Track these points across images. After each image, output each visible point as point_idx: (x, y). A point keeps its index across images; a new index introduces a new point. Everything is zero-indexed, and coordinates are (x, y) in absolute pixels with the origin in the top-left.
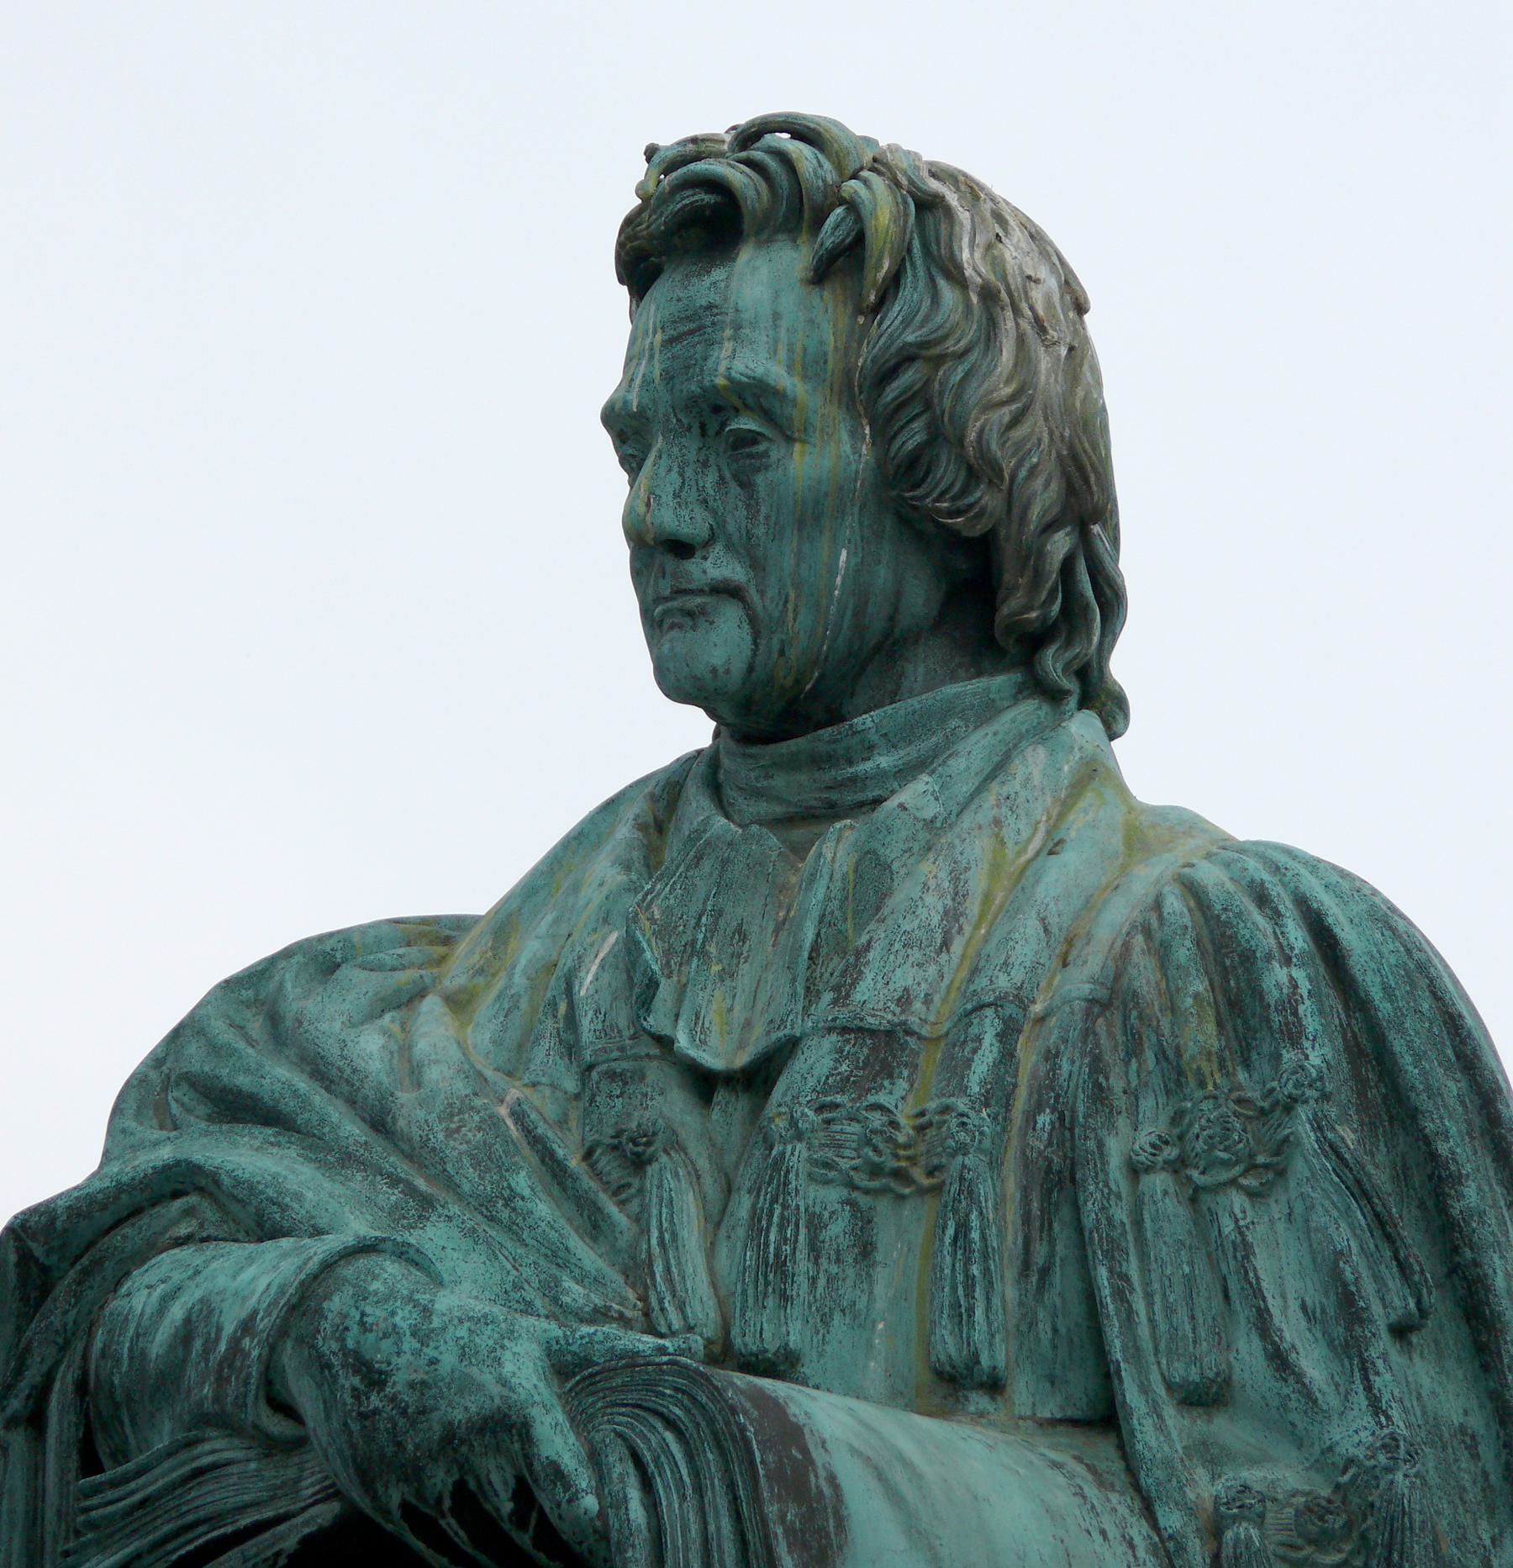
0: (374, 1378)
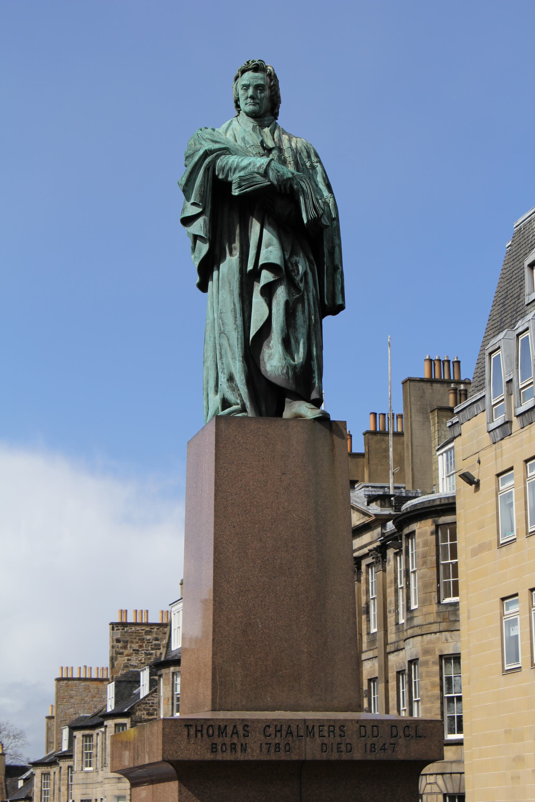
0: (279, 172)
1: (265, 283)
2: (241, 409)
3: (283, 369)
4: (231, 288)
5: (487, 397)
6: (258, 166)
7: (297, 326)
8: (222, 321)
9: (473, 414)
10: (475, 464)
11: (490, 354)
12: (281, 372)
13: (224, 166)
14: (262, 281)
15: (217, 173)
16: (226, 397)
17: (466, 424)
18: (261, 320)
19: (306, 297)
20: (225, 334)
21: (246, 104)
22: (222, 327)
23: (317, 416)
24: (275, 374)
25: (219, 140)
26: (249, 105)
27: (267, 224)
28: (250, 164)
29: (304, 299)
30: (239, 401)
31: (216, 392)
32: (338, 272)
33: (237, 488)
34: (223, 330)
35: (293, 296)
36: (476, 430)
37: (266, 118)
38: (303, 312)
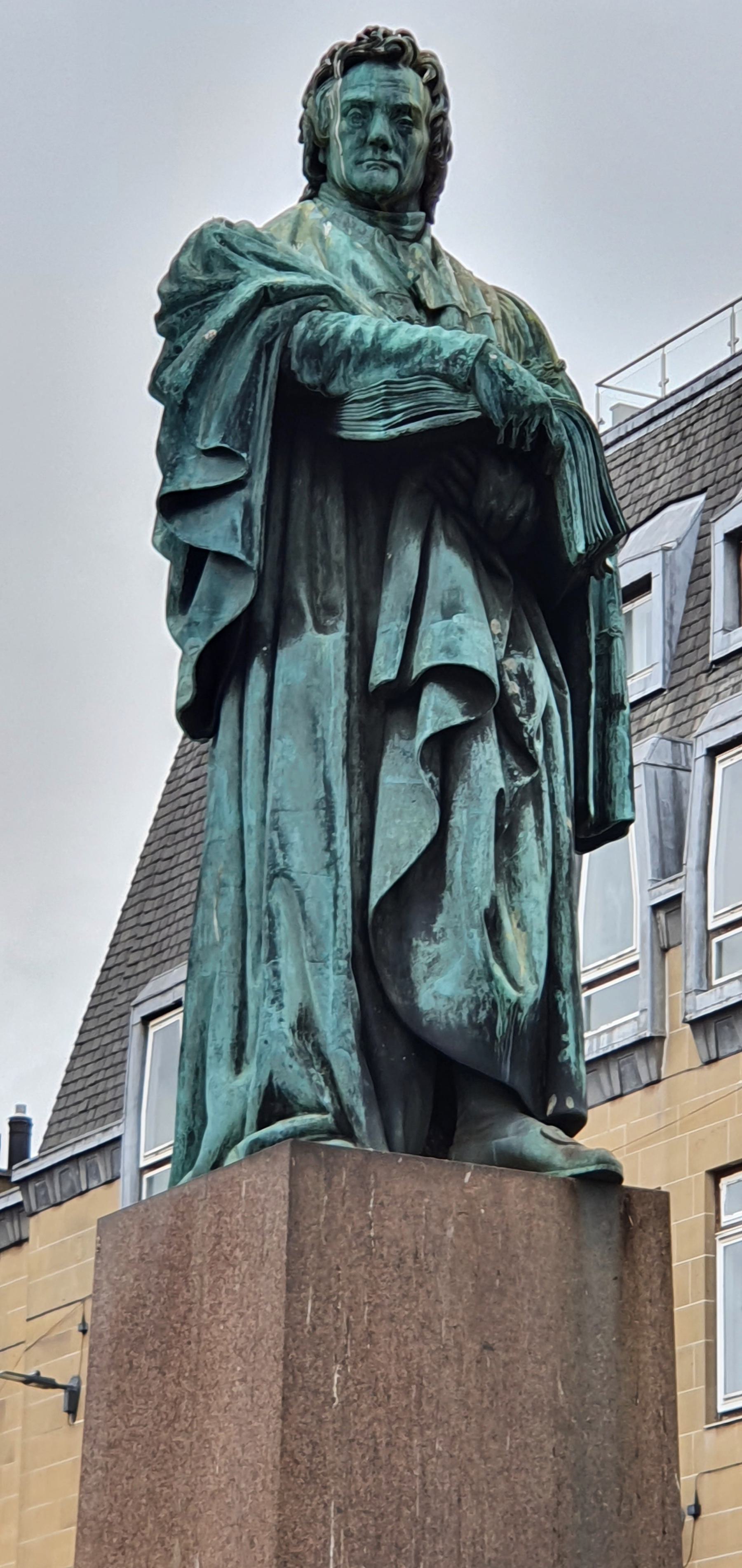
0: (511, 382)
1: (437, 729)
2: (334, 1127)
3: (478, 1007)
4: (319, 735)
5: (127, 1143)
6: (446, 354)
7: (520, 876)
8: (280, 836)
9: (73, 1189)
10: (70, 1332)
11: (146, 1020)
12: (470, 1016)
13: (327, 345)
14: (429, 723)
15: (295, 364)
16: (277, 1081)
17: (47, 1216)
18: (411, 846)
19: (545, 786)
20: (291, 880)
21: (358, 163)
22: (279, 854)
23: (592, 1168)
24: (448, 1024)
25: (291, 263)
26: (369, 167)
27: (442, 543)
28: (419, 346)
29: (540, 791)
30: (326, 1100)
31: (238, 1064)
32: (621, 718)
33: (350, 1383)
34: (282, 866)
35: (514, 778)
36: (79, 1237)
37: (409, 214)
38: (540, 831)
